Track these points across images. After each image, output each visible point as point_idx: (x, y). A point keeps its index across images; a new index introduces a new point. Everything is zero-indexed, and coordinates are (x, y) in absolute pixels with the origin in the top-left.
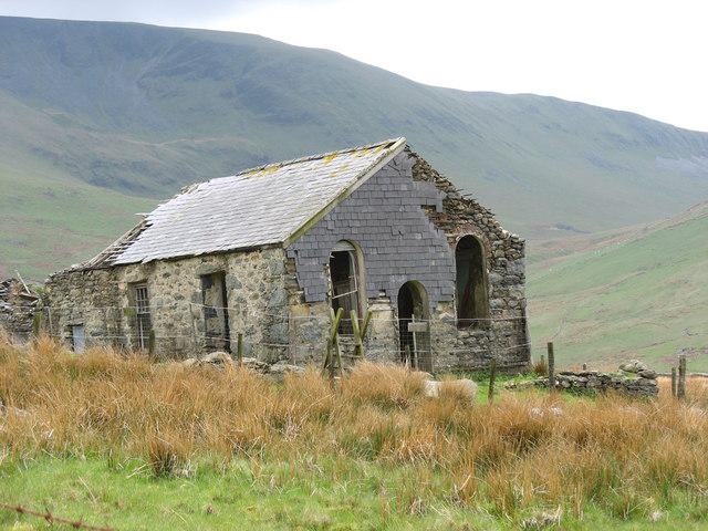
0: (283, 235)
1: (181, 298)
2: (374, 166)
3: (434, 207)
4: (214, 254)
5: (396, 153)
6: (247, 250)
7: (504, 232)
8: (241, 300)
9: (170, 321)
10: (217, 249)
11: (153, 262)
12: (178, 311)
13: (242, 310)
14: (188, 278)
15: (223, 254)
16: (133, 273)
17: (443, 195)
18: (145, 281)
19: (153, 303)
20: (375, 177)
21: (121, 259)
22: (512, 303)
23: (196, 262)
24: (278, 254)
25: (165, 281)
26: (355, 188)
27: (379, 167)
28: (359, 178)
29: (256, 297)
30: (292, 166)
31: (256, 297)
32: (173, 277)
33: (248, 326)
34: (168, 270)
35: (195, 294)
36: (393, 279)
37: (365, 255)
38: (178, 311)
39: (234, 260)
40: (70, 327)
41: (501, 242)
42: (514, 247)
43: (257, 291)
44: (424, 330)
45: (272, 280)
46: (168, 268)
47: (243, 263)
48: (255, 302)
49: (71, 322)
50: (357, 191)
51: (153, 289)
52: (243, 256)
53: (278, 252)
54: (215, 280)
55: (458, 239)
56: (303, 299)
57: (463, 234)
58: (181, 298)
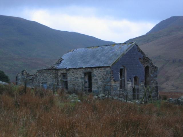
0: (110, 64)
1: (77, 78)
2: (129, 48)
3: (141, 58)
4: (89, 68)
5: (134, 45)
6: (99, 67)
7: (154, 65)
8: (96, 80)
9: (73, 83)
10: (90, 66)
11: (69, 69)
12: (76, 81)
13: (96, 82)
14: (80, 74)
15: (91, 68)
16: (63, 71)
17: (142, 56)
18: (66, 73)
19: (69, 78)
20: (129, 51)
21: (58, 67)
22: (155, 82)
23: (83, 69)
24: (108, 69)
25: (73, 73)
26: (125, 53)
27: (130, 48)
28: (126, 51)
29: (101, 79)
30: (102, 47)
31: (101, 79)
32: (75, 73)
33: (98, 86)
34: (73, 71)
35: (82, 77)
36: (132, 76)
37: (127, 70)
38: (76, 81)
39: (94, 70)
40: (43, 83)
41: (153, 67)
42: (155, 68)
43: (101, 77)
44: (138, 88)
45: (106, 75)
46: (74, 71)
47: (97, 70)
48: (101, 80)
49: (43, 82)
50: (126, 54)
51: (68, 75)
52: (98, 69)
53: (108, 68)
54: (89, 75)
55: (145, 66)
56: (114, 80)
57: (146, 65)
58: (77, 78)
